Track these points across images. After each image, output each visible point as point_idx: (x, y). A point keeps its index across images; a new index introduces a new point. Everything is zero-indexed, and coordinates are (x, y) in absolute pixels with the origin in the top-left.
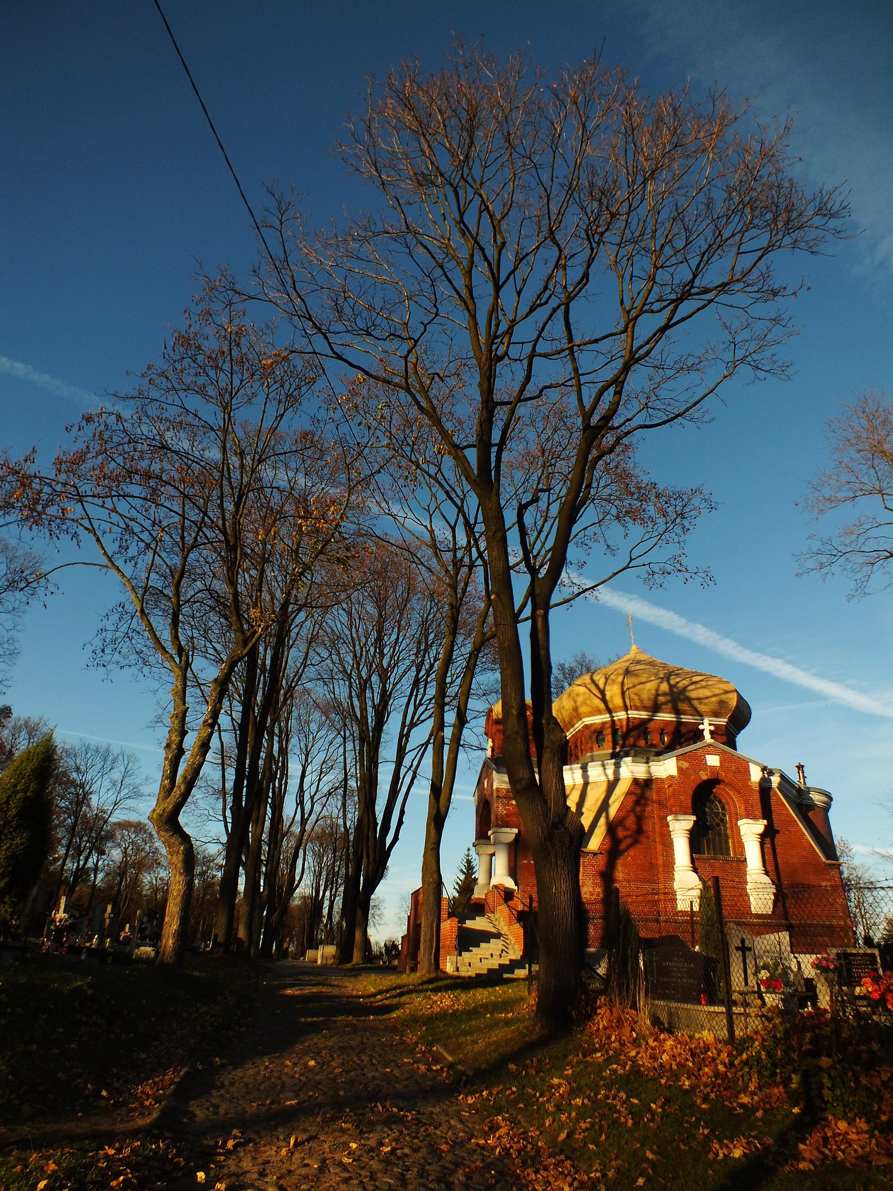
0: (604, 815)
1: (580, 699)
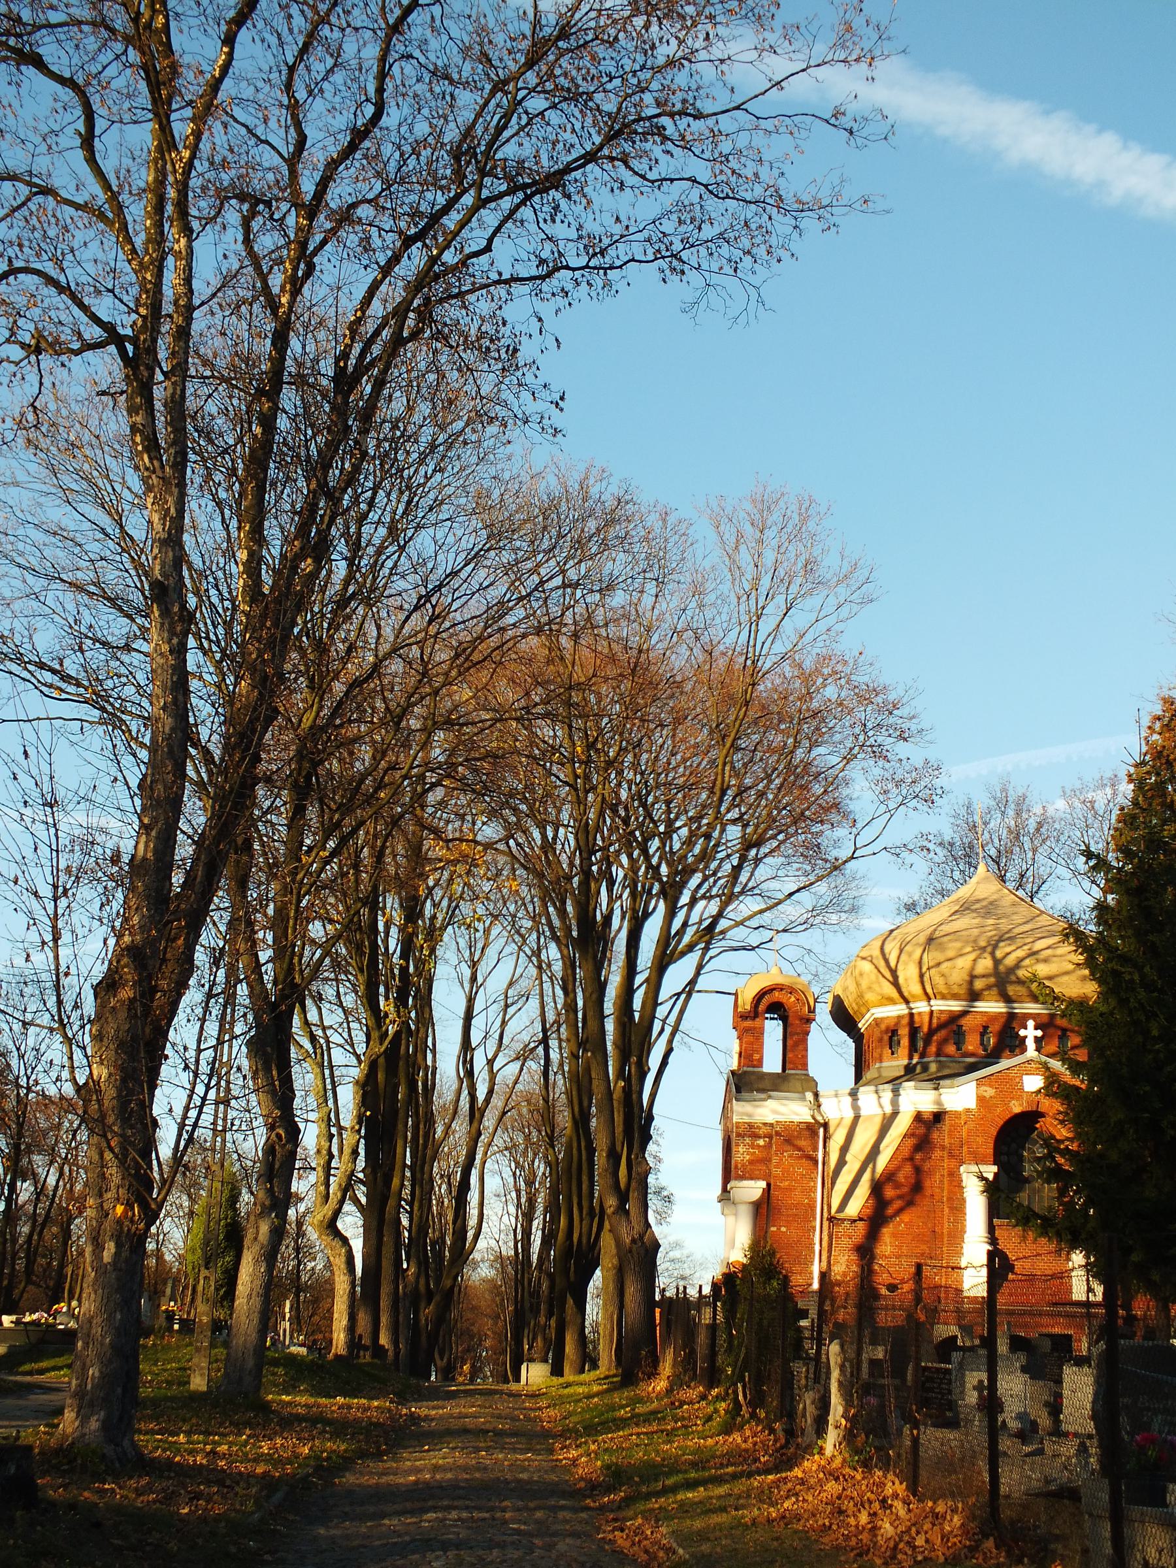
0: (869, 1170)
1: (864, 984)
